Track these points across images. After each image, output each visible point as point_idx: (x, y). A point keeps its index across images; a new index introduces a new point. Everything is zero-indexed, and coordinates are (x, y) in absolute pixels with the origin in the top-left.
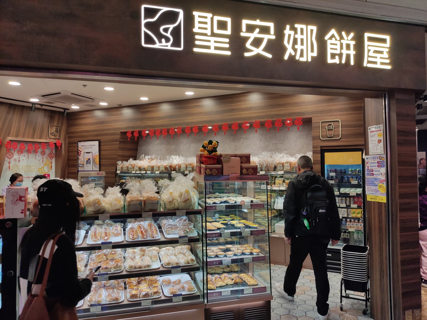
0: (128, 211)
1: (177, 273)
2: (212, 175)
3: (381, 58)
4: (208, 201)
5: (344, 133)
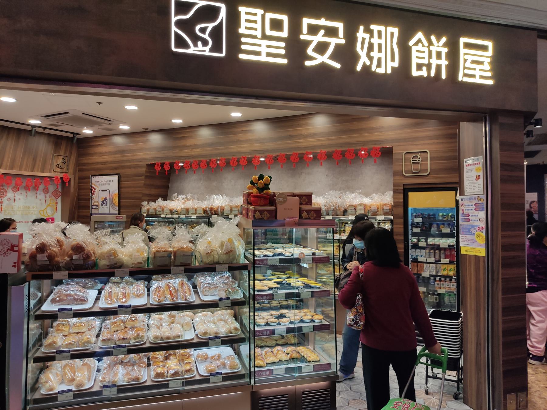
0: (154, 264)
1: (216, 345)
2: (262, 219)
3: (481, 70)
4: (257, 253)
5: (433, 168)
